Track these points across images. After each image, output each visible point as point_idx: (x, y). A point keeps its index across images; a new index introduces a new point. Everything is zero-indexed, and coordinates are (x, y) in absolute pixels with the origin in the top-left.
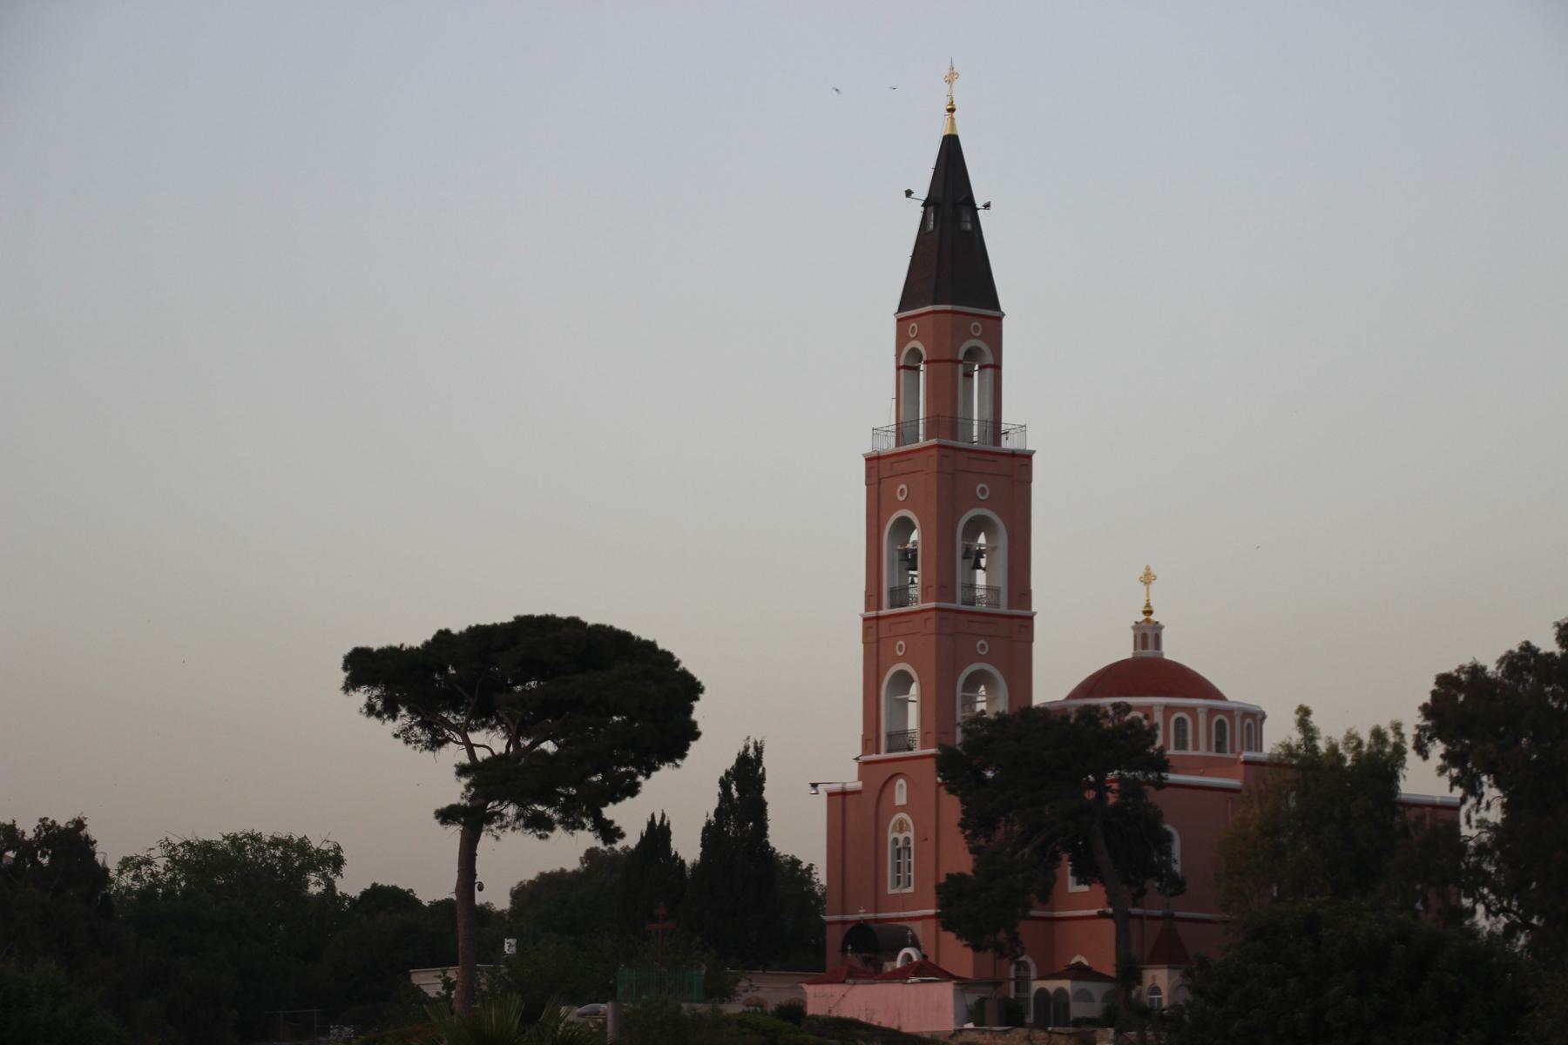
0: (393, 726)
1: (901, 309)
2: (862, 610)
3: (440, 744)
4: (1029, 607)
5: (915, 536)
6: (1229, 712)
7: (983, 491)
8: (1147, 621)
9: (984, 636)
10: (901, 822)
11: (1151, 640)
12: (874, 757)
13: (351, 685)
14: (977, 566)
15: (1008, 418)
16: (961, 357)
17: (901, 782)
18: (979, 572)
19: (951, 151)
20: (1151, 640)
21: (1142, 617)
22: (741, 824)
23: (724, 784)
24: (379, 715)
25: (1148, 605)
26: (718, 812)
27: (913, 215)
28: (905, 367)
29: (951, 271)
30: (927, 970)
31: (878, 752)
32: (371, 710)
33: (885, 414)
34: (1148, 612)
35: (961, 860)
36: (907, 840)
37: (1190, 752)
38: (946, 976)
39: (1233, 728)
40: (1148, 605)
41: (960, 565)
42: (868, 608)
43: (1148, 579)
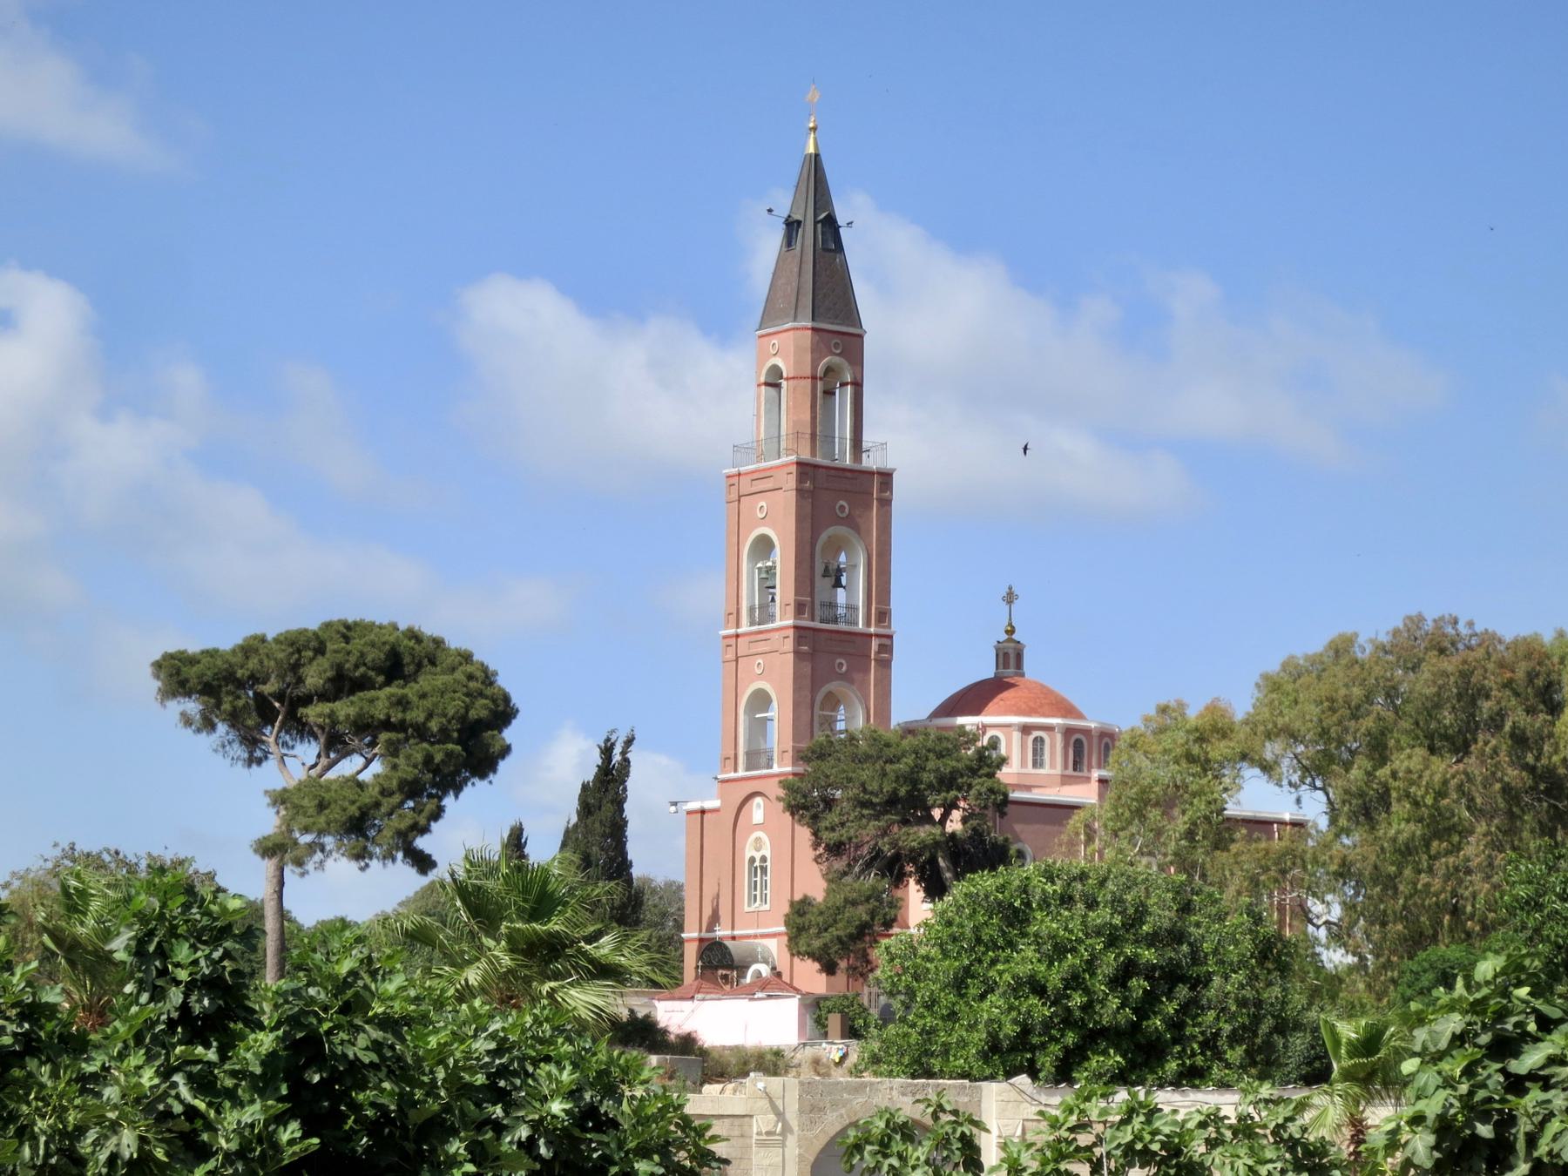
4: (889, 627)
6: (1087, 732)
7: (842, 507)
8: (1010, 640)
9: (841, 654)
10: (758, 839)
11: (1012, 661)
12: (732, 775)
14: (838, 584)
15: (868, 438)
17: (758, 800)
18: (840, 590)
20: (1012, 661)
21: (1005, 637)
25: (1010, 624)
28: (767, 384)
30: (776, 985)
31: (736, 770)
32: (187, 721)
34: (1011, 631)
35: (813, 884)
36: (764, 859)
38: (797, 990)
39: (1053, 746)
40: (1010, 624)
41: (822, 584)
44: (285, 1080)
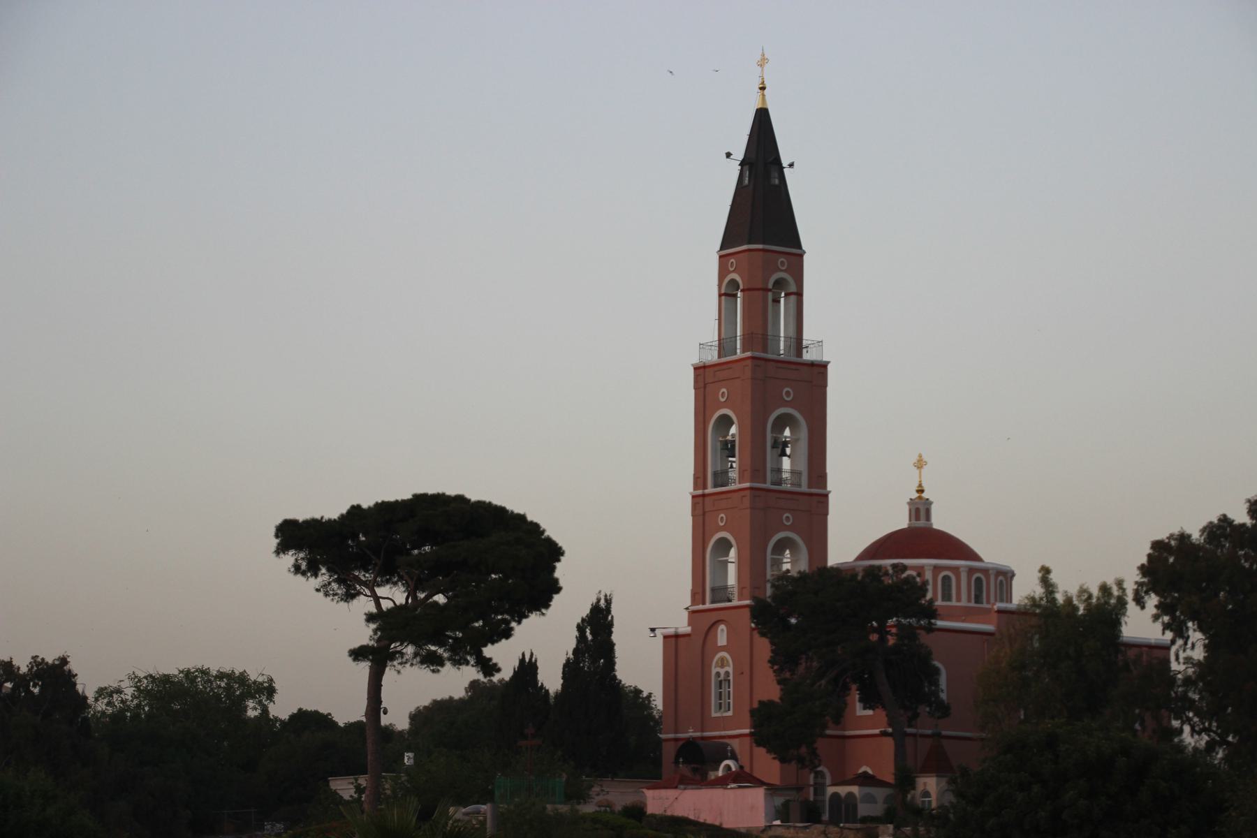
0: (315, 582)
1: (722, 248)
2: (691, 489)
3: (353, 596)
4: (825, 487)
5: (733, 430)
6: (985, 571)
7: (788, 394)
8: (920, 498)
9: (789, 510)
10: (722, 659)
11: (923, 514)
12: (701, 607)
13: (282, 549)
14: (783, 454)
15: (808, 336)
16: (770, 286)
17: (722, 627)
18: (785, 459)
19: (762, 121)
20: (923, 514)
21: (916, 495)
22: (594, 660)
23: (581, 629)
24: (304, 573)
25: (920, 485)
26: (575, 651)
27: (732, 172)
28: (725, 294)
29: (762, 217)
30: (743, 778)
31: (704, 603)
32: (297, 569)
33: (710, 332)
34: (921, 491)
36: (727, 673)
37: (954, 603)
38: (758, 783)
39: (988, 584)
40: (920, 485)
41: (770, 453)
42: (695, 488)
43: (920, 464)
44: (1172, 740)
